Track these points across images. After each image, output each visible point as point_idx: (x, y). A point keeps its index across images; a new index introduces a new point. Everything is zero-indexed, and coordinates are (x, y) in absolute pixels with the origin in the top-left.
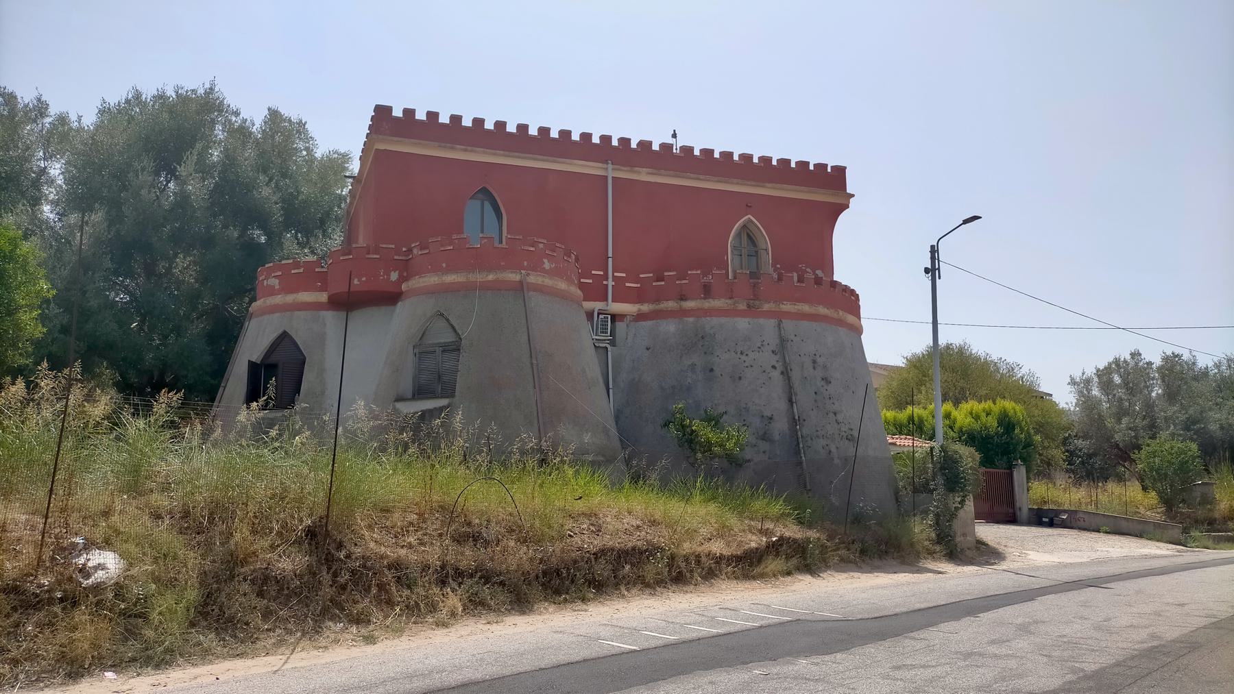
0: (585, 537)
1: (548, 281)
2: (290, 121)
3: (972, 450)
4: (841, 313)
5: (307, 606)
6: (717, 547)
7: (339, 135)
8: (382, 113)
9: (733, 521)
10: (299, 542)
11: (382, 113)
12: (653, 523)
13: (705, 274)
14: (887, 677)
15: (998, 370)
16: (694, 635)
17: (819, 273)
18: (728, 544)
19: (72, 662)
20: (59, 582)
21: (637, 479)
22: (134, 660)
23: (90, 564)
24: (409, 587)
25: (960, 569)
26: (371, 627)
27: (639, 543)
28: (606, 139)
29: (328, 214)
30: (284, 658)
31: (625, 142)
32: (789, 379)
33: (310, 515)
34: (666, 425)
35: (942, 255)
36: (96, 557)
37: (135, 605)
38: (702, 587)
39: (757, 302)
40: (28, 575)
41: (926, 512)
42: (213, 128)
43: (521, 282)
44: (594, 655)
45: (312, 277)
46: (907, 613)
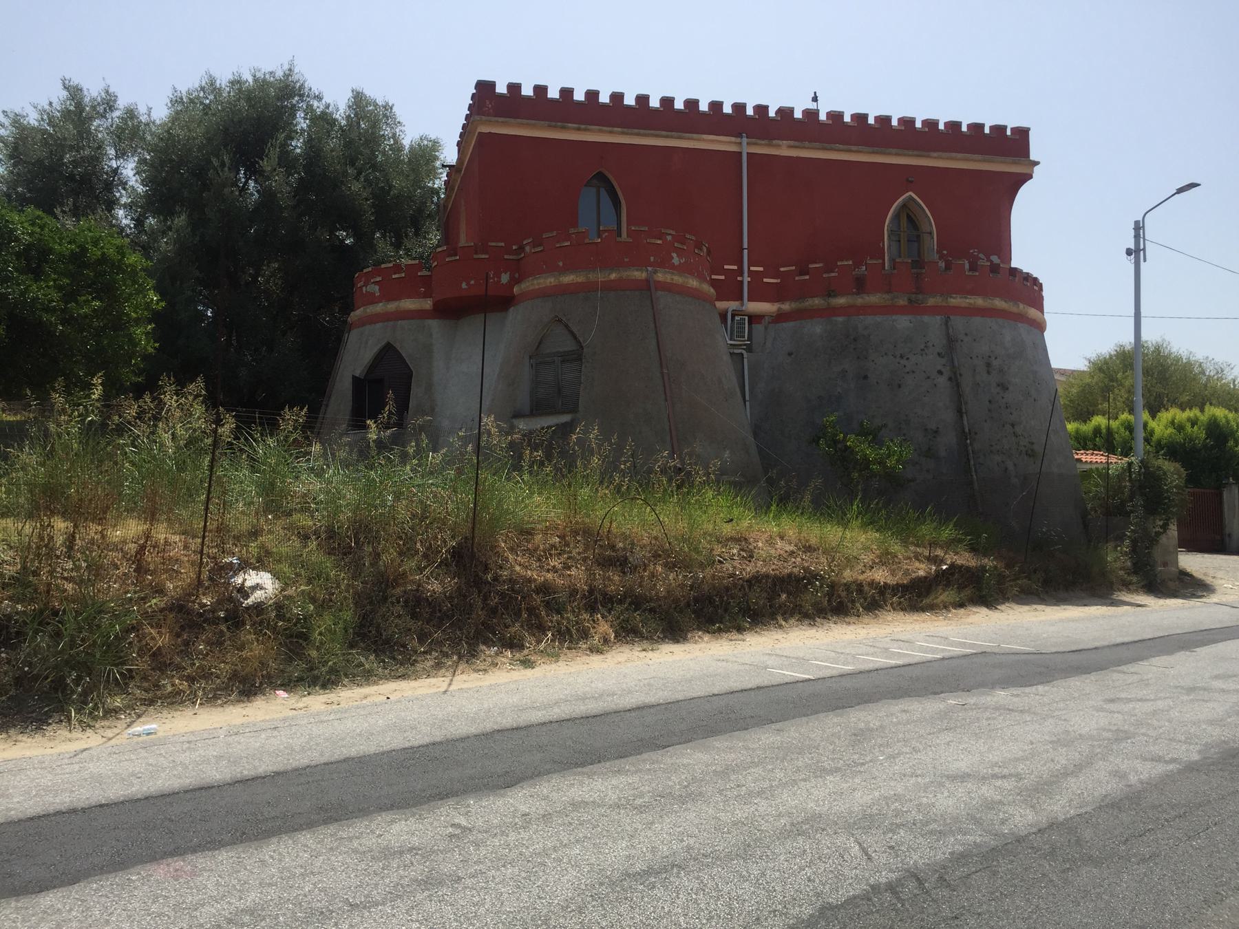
0: (736, 564)
1: (678, 279)
2: (376, 105)
3: (1178, 465)
4: (1021, 306)
5: (461, 629)
6: (881, 575)
7: (432, 120)
8: (484, 89)
9: (896, 548)
10: (445, 563)
11: (484, 89)
12: (809, 549)
13: (857, 264)
14: (1101, 710)
15: (1203, 373)
16: (871, 666)
17: (995, 259)
18: (893, 573)
19: (243, 680)
20: (219, 602)
21: (783, 501)
22: (300, 679)
23: (248, 584)
24: (558, 612)
25: (1162, 602)
26: (526, 652)
27: (796, 570)
28: (739, 108)
29: (420, 211)
30: (447, 680)
31: (716, 106)
32: (958, 385)
33: (453, 537)
34: (815, 441)
35: (1150, 232)
36: (252, 578)
37: (295, 625)
38: (866, 619)
39: (920, 296)
40: (190, 595)
41: (1121, 538)
42: (294, 116)
43: (647, 281)
44: (766, 683)
45: (414, 283)
46: (1108, 646)
